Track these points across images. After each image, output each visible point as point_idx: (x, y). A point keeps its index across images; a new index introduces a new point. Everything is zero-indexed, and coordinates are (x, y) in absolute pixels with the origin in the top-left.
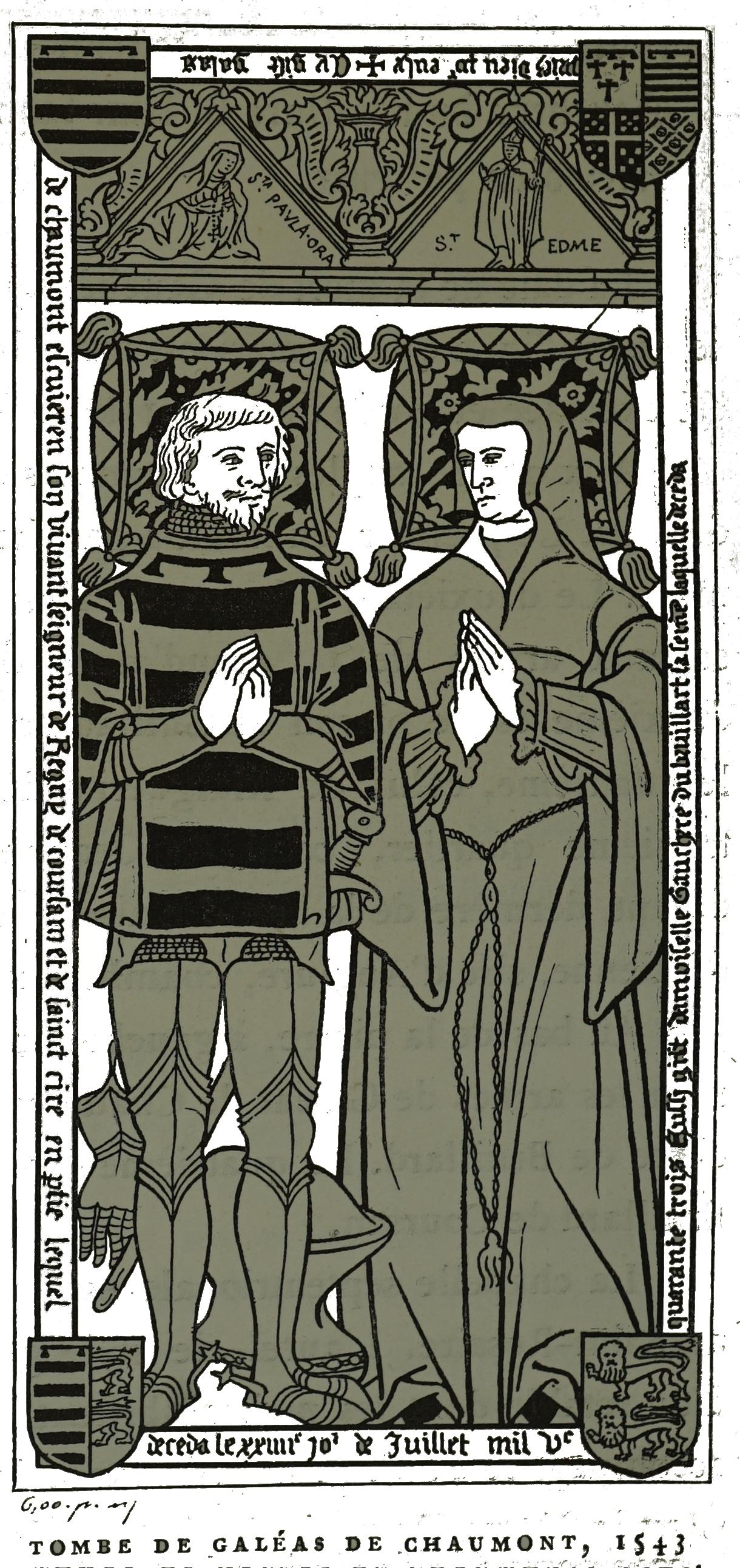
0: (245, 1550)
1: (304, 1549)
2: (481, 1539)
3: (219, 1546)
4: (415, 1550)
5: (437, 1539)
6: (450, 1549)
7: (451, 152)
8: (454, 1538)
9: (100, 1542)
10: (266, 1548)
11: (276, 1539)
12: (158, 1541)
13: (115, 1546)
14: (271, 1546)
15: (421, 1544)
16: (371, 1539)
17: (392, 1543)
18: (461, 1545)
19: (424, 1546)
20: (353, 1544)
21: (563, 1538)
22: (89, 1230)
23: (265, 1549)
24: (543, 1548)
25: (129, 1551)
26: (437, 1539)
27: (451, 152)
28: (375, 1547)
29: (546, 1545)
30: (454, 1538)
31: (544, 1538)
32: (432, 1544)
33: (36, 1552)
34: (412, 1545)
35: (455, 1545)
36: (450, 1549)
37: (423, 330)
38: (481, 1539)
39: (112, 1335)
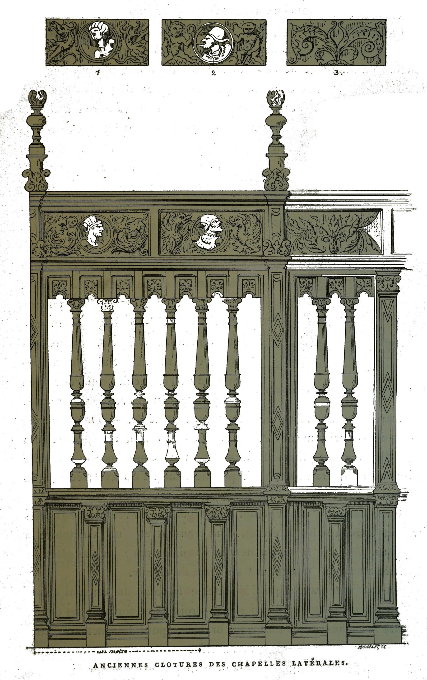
0: (326, 665)
1: (249, 666)
2: (183, 663)
3: (156, 665)
4: (158, 666)
5: (242, 662)
6: (246, 666)
7: (343, 33)
8: (247, 662)
9: (187, 663)
10: (268, 665)
11: (311, 662)
12: (210, 663)
13: (192, 665)
14: (335, 663)
15: (237, 664)
16: (217, 663)
17: (228, 664)
18: (98, 666)
19: (316, 664)
20: (211, 664)
21: (174, 663)
22: (249, 503)
23: (295, 665)
24: (125, 667)
25: (121, 667)
26: (242, 662)
27: (343, 33)
28: (278, 664)
29: (126, 666)
30: (247, 662)
31: (125, 664)
32: (241, 664)
33: (175, 666)
34: (157, 665)
35: (248, 664)
36: (246, 666)
37: (150, 59)
38: (183, 663)
39: (397, 571)
